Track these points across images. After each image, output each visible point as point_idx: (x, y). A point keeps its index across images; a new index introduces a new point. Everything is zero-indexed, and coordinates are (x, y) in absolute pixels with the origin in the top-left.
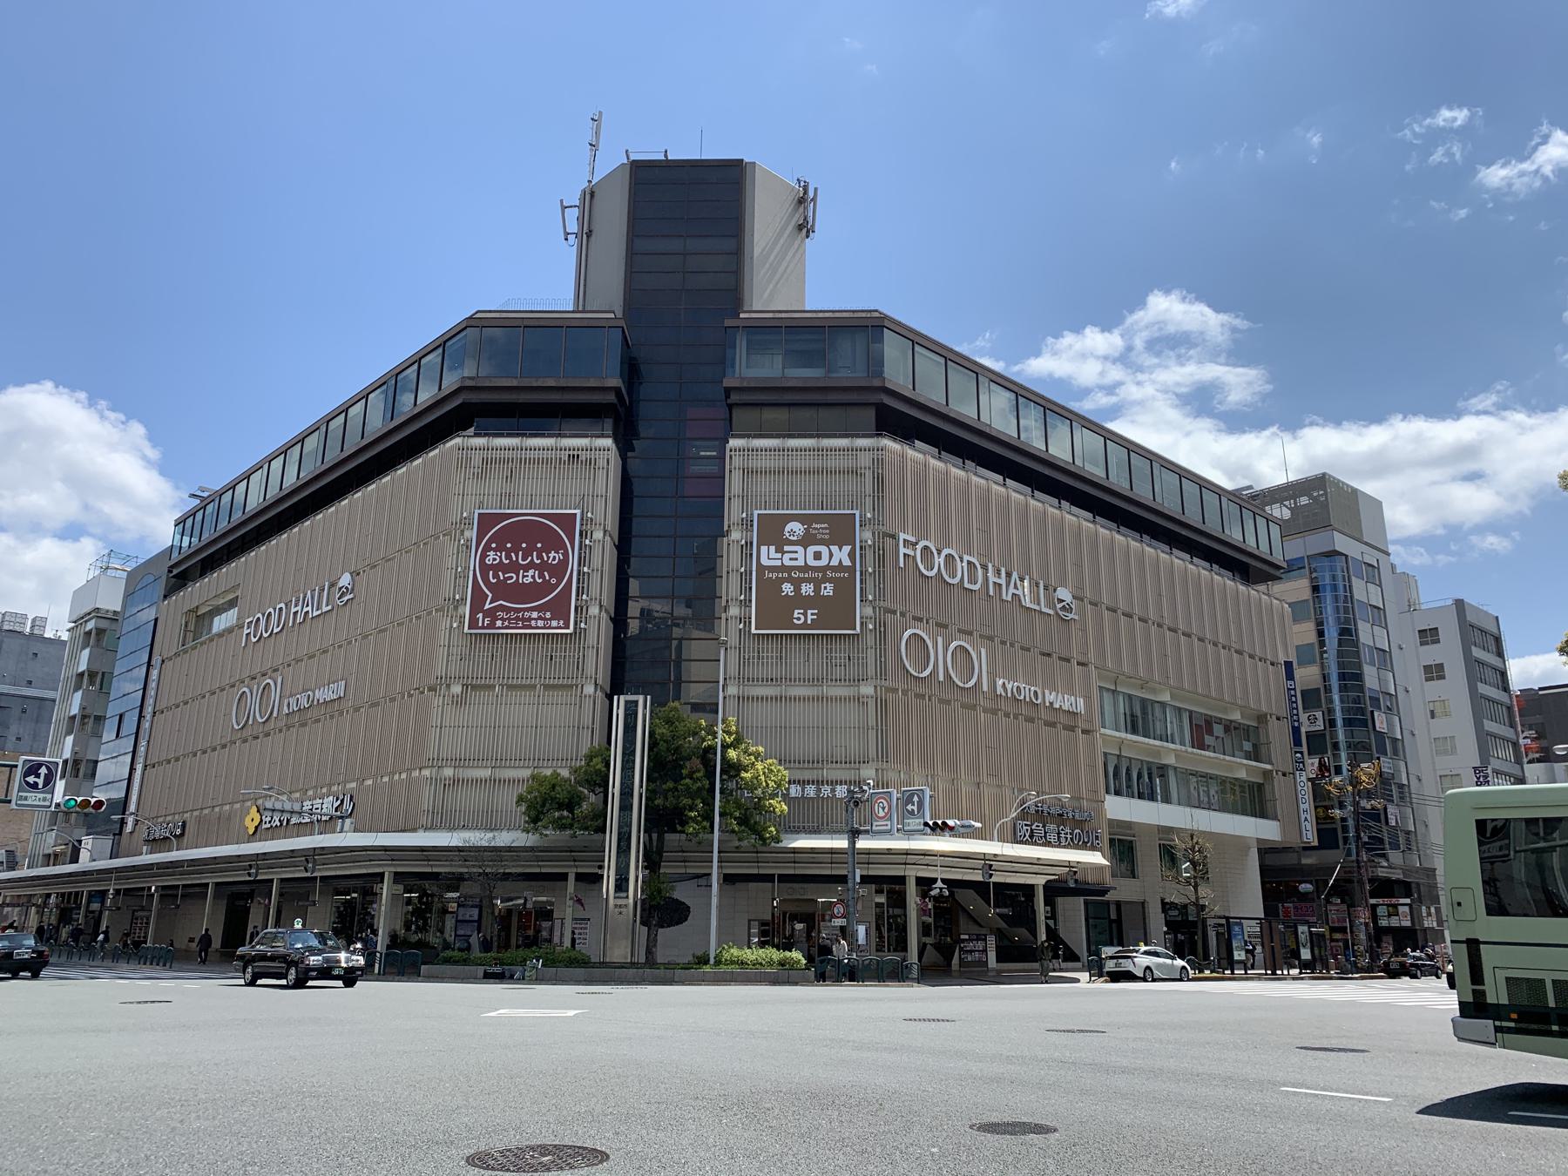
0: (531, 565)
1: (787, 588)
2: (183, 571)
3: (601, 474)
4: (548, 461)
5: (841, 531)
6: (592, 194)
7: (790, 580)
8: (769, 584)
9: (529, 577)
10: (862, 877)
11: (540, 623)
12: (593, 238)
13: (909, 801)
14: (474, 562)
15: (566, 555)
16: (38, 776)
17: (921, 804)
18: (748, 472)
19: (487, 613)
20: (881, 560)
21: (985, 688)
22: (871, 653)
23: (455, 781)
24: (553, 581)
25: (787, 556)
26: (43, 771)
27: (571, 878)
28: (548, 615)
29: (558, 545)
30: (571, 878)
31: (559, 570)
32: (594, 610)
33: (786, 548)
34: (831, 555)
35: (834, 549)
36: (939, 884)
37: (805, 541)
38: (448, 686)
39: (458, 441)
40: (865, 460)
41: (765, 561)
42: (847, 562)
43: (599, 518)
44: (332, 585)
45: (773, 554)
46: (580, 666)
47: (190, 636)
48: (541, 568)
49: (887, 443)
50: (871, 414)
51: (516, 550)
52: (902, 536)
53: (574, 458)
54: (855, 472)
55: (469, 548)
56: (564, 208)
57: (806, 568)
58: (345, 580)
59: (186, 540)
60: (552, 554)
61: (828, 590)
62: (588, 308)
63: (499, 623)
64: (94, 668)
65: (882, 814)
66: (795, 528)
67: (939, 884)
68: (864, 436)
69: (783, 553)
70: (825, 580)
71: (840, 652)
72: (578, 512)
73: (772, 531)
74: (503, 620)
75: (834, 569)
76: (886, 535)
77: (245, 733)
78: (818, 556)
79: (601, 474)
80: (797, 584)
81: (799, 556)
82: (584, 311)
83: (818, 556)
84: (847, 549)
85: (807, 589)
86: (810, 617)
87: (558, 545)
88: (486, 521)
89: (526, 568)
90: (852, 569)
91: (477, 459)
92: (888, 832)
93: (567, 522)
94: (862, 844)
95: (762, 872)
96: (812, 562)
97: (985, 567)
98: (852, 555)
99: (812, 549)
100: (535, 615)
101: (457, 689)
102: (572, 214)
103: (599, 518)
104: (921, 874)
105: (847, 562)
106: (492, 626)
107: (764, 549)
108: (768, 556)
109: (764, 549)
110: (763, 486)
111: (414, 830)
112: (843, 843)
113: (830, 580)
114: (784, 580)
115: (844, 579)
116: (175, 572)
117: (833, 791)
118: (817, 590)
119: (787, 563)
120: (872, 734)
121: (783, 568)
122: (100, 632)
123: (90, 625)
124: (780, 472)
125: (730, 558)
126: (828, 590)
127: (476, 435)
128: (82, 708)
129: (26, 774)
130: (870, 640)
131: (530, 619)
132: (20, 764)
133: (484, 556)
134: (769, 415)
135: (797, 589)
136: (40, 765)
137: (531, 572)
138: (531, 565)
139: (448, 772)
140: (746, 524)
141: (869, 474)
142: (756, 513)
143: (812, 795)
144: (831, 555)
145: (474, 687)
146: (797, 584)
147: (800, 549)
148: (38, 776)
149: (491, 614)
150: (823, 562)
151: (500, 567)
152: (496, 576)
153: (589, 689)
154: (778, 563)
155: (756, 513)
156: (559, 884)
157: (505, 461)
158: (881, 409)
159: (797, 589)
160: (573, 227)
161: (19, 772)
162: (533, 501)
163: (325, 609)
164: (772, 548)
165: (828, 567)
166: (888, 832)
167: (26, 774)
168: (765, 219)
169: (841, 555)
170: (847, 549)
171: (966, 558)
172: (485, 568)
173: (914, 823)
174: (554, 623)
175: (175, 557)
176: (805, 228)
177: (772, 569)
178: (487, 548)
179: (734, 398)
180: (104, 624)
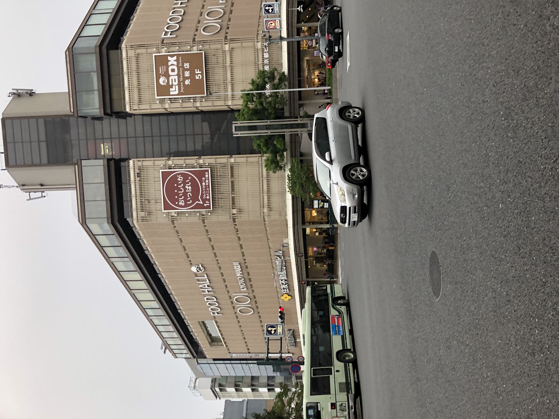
0: (184, 187)
1: (187, 82)
2: (196, 351)
3: (145, 163)
4: (140, 185)
5: (162, 61)
6: (23, 185)
7: (184, 81)
8: (185, 90)
9: (189, 188)
10: (297, 36)
11: (207, 181)
12: (44, 183)
13: (267, 11)
14: (184, 210)
15: (179, 174)
16: (272, 330)
17: (270, 6)
18: (140, 102)
19: (204, 202)
20: (173, 44)
21: (224, 6)
22: (213, 47)
23: (269, 207)
24: (190, 178)
25: (174, 83)
26: (270, 329)
27: (302, 158)
28: (204, 179)
29: (175, 177)
30: (302, 158)
31: (185, 176)
32: (201, 161)
33: (171, 84)
34: (172, 65)
35: (170, 63)
36: (299, 9)
37: (167, 76)
38: (233, 214)
39: (135, 222)
40: (132, 53)
41: (177, 92)
42: (175, 58)
43: (163, 162)
44: (197, 276)
45: (174, 89)
46: (224, 166)
47: (219, 343)
48: (184, 183)
49: (123, 45)
50: (112, 52)
51: (178, 194)
52: (163, 36)
53: (139, 175)
54: (137, 57)
55: (178, 213)
56: (30, 199)
57: (178, 75)
58: (194, 269)
59: (185, 351)
60: (179, 179)
61: (187, 65)
62: (75, 183)
63: (208, 197)
64: (233, 385)
65: (273, 24)
66: (162, 80)
67: (299, 9)
68: (121, 54)
69: (172, 85)
70: (183, 67)
71: (212, 60)
72: (161, 171)
73: (164, 90)
74: (206, 196)
75: (178, 63)
76: (163, 43)
77: (255, 308)
78: (173, 70)
79: (145, 163)
80: (185, 78)
81: (174, 78)
82: (76, 187)
83: (173, 70)
84: (169, 58)
85: (187, 74)
86: (199, 72)
87: (175, 177)
88: (167, 207)
89: (185, 189)
90: (178, 56)
91: (142, 214)
92: (280, 21)
93: (165, 175)
94: (284, 34)
95: (300, 209)
96: (176, 73)
97: (174, 8)
98: (172, 56)
99: (170, 73)
100: (204, 184)
101: (235, 211)
102: (33, 195)
103: (163, 162)
104: (296, 22)
105: (175, 58)
106: (209, 200)
107: (171, 93)
108: (174, 91)
109: (171, 93)
110: (146, 96)
111: (287, 220)
112: (285, 44)
113: (183, 64)
114: (184, 84)
115: (182, 59)
116: (195, 355)
117: (266, 59)
118: (187, 70)
119: (177, 83)
120: (244, 44)
121: (179, 85)
122: (220, 385)
123: (217, 389)
124: (138, 74)
125: (176, 107)
126: (187, 65)
127: (132, 217)
128: (248, 387)
129: (271, 334)
130: (207, 47)
131: (206, 186)
132: (267, 337)
133: (181, 206)
134: (115, 96)
135: (187, 78)
136: (268, 331)
137: (187, 187)
138: (184, 187)
139: (266, 210)
140: (162, 101)
141: (138, 51)
142: (163, 211)
143: (268, 67)
144: (172, 65)
145: (233, 203)
146: (185, 78)
147: (171, 78)
148: (272, 330)
149: (204, 201)
150: (175, 68)
151: (185, 200)
152: (189, 201)
153: (232, 160)
154: (177, 87)
155: (157, 97)
156: (302, 95)
157: (142, 203)
158: (109, 48)
159: (187, 78)
160: (39, 194)
161: (271, 337)
162: (157, 190)
163: (206, 277)
164: (171, 89)
165: (177, 66)
166: (280, 21)
167: (271, 334)
168: (27, 108)
169: (172, 60)
170: (169, 58)
171: (171, 14)
172: (186, 205)
173: (276, 9)
174: (207, 176)
175: (189, 356)
176: (31, 94)
177: (180, 89)
178: (178, 205)
179: (109, 111)
180: (217, 384)
